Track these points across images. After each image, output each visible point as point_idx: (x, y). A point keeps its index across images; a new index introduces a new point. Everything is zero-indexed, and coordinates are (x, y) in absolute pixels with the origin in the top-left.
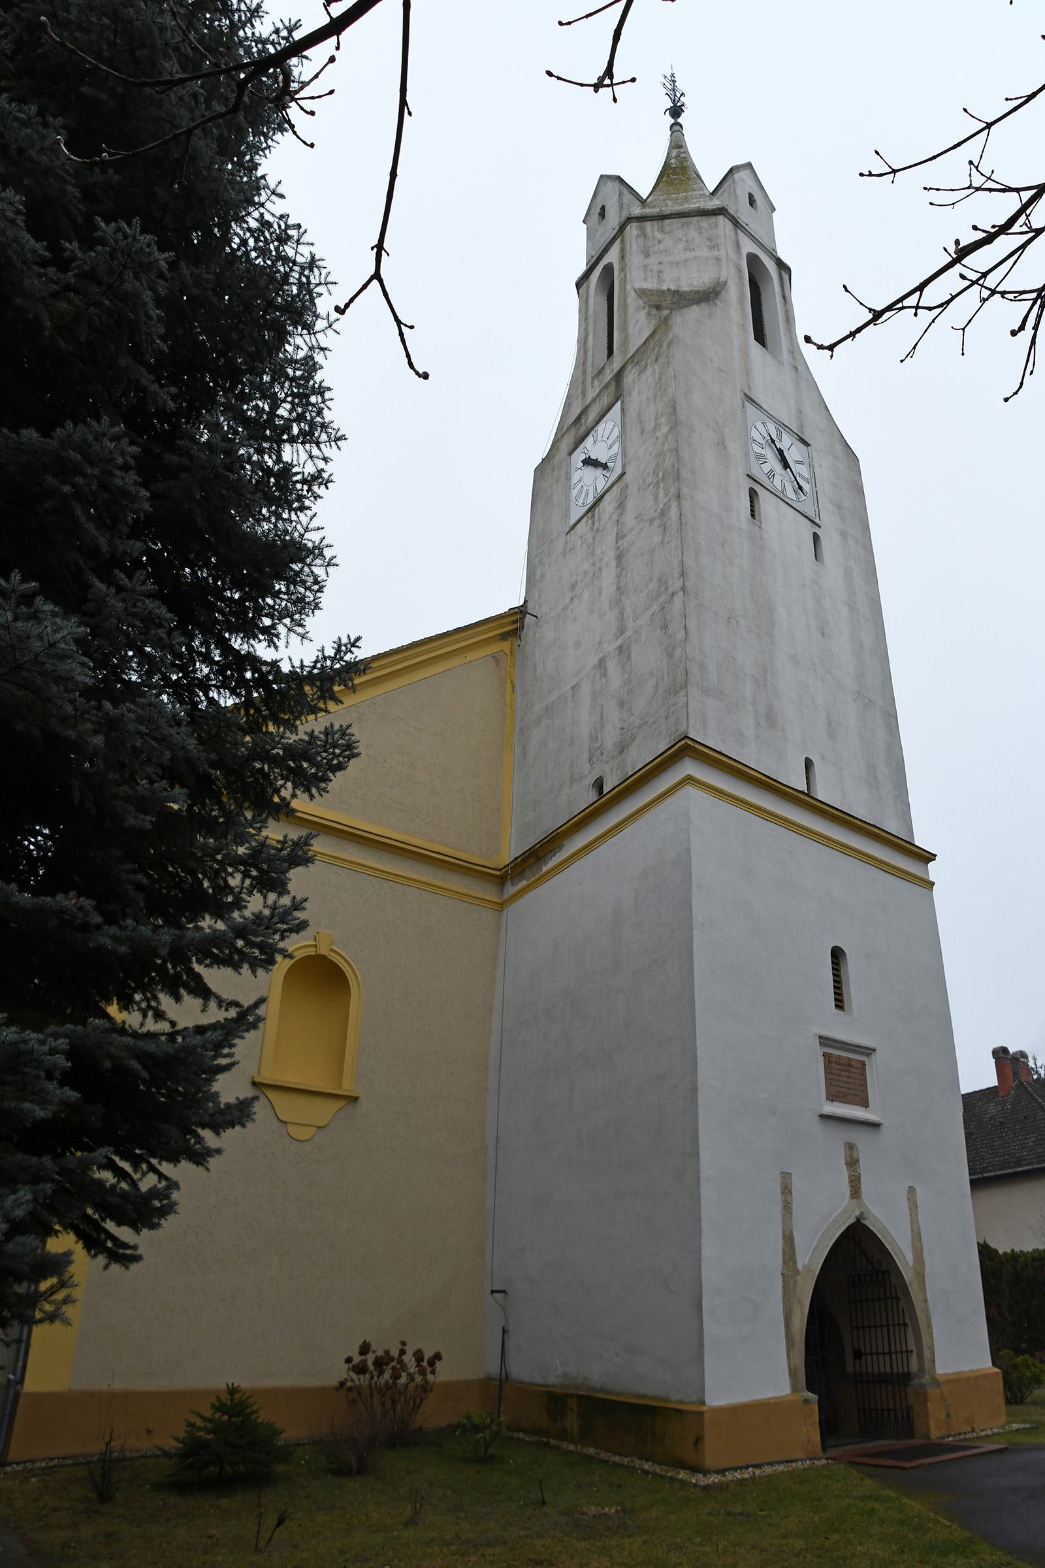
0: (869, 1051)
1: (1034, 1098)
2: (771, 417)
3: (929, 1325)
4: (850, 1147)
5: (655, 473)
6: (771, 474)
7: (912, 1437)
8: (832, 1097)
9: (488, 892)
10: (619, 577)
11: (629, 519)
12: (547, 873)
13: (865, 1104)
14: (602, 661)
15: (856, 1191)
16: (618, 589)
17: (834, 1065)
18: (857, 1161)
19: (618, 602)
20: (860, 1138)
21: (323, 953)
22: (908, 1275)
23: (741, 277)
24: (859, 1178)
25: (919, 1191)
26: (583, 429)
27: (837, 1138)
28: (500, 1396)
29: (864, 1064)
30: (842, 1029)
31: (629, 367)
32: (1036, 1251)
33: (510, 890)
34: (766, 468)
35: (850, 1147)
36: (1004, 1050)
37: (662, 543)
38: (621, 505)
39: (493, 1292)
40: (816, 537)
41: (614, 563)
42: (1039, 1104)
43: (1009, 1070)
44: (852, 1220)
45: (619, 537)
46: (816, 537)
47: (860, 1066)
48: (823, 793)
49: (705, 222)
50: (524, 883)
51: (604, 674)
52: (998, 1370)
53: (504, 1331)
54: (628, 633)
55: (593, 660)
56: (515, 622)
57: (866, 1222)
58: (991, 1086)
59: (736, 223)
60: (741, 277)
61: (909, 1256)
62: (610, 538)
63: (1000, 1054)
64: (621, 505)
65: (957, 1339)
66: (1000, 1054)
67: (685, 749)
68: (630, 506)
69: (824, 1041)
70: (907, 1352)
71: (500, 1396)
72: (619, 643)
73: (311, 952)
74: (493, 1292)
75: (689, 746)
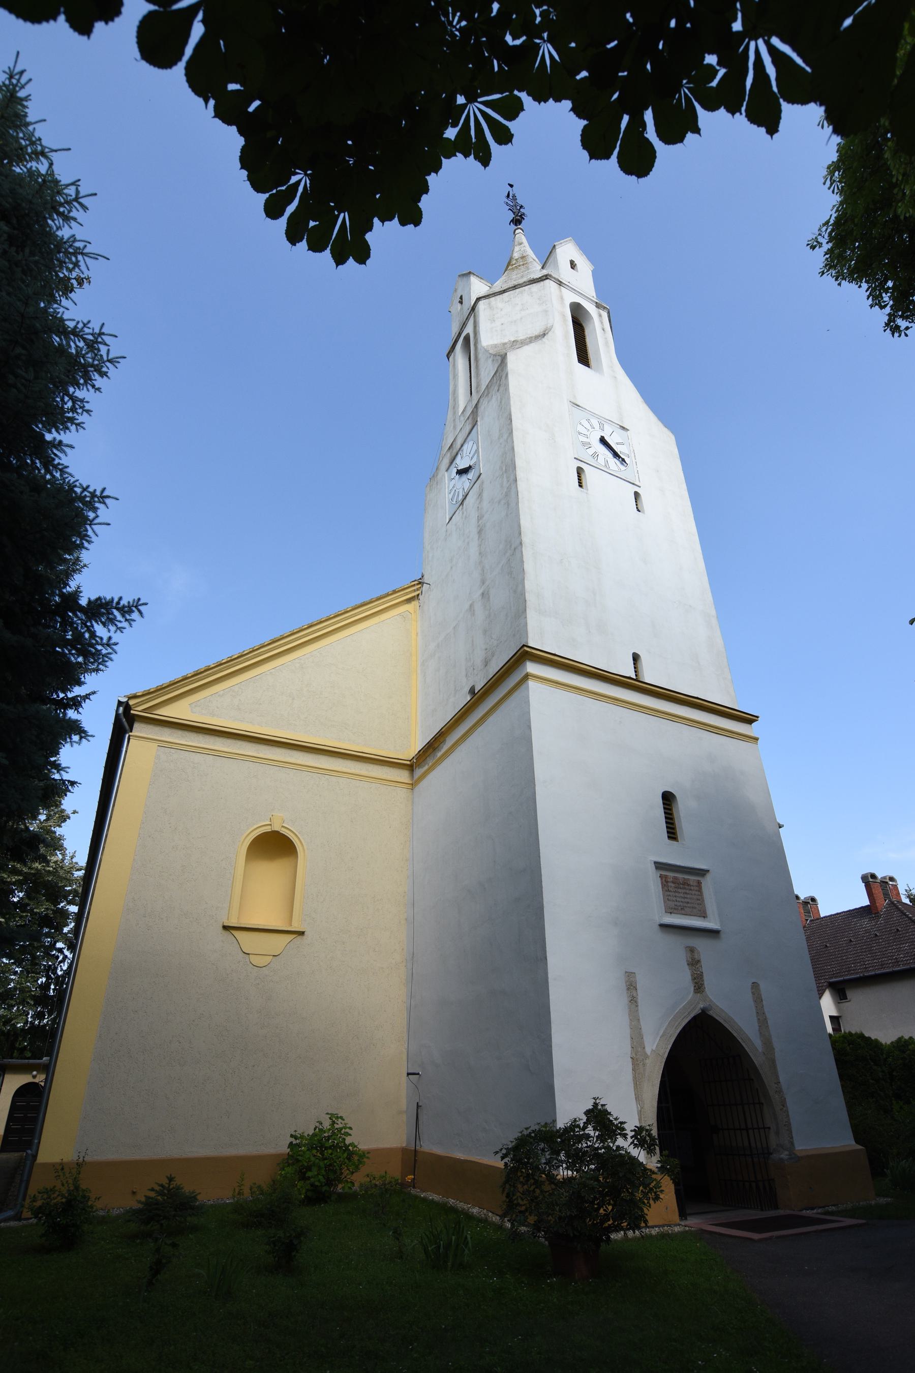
0: (703, 873)
1: (905, 914)
2: (594, 414)
3: (784, 1104)
4: (692, 950)
5: (501, 468)
6: (595, 455)
7: (776, 1207)
8: (670, 911)
9: (403, 776)
10: (480, 545)
11: (485, 504)
12: (440, 758)
13: (704, 915)
14: (471, 606)
15: (699, 985)
16: (480, 553)
17: (670, 884)
18: (699, 961)
19: (481, 562)
20: (702, 945)
21: (276, 829)
22: (758, 1060)
23: (565, 320)
24: (701, 975)
25: (763, 986)
26: (455, 451)
27: (679, 943)
28: (415, 1160)
29: (699, 883)
30: (673, 855)
31: (481, 400)
32: (876, 1040)
33: (418, 772)
34: (591, 451)
35: (692, 950)
36: (873, 876)
37: (507, 515)
38: (480, 495)
39: (408, 1074)
40: (637, 495)
41: (476, 537)
42: (910, 919)
43: (878, 892)
44: (697, 1011)
45: (480, 518)
46: (637, 495)
47: (695, 884)
48: (650, 676)
49: (535, 287)
50: (426, 767)
51: (473, 614)
52: (860, 1147)
53: (418, 1106)
54: (487, 583)
55: (467, 606)
56: (418, 590)
57: (711, 1013)
58: (864, 905)
59: (560, 283)
60: (565, 320)
61: (758, 1043)
62: (474, 520)
63: (869, 880)
64: (480, 495)
65: (814, 1120)
66: (869, 880)
67: (525, 654)
68: (485, 495)
69: (659, 866)
70: (764, 1128)
71: (415, 1160)
72: (481, 591)
73: (268, 829)
74: (408, 1074)
75: (527, 652)
